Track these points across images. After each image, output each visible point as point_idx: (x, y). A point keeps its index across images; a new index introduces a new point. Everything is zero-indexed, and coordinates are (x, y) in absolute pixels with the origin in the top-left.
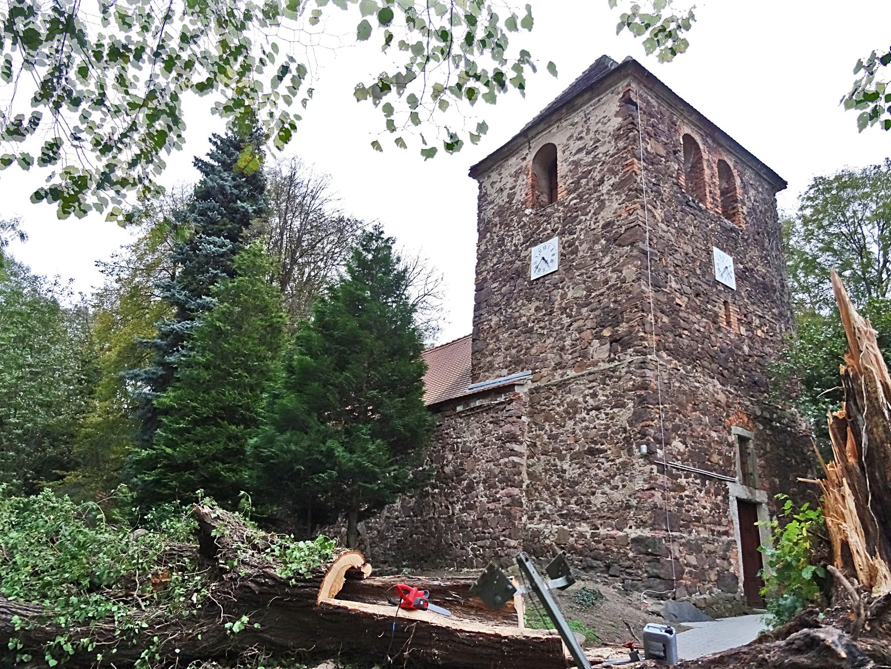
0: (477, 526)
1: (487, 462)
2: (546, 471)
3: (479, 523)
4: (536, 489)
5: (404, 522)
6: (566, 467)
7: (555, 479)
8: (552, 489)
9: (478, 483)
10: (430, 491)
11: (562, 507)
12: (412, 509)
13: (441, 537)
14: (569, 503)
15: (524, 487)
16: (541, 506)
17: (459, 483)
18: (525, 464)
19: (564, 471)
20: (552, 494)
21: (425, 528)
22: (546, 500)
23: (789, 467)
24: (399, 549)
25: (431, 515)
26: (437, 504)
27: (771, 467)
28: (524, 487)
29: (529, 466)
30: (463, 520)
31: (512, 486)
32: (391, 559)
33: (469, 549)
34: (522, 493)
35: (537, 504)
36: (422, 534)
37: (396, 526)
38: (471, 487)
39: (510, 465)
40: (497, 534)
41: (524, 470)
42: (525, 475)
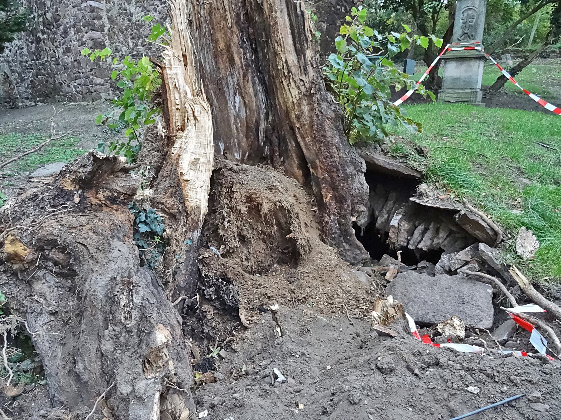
0: (75, 67)
1: (73, 7)
2: (120, 14)
3: (76, 64)
4: (115, 33)
5: (31, 65)
6: (132, 10)
7: (126, 22)
8: (125, 32)
9: (70, 27)
10: (41, 37)
11: (133, 49)
12: (34, 54)
13: (54, 77)
14: (137, 45)
15: (106, 31)
16: (119, 48)
17: (58, 28)
18: (104, 9)
19: (131, 15)
20: (125, 38)
21: (44, 69)
22: (122, 43)
23: (338, 14)
24: (32, 87)
25: (46, 59)
26: (48, 49)
27: (321, 13)
28: (106, 31)
29: (108, 11)
30: (66, 63)
31: (92, 30)
32: (30, 96)
33: (72, 86)
34: (104, 36)
35: (116, 46)
36: (44, 75)
37: (27, 69)
38: (66, 32)
39: (88, 9)
40: (88, 73)
41: (104, 14)
42: (105, 20)
